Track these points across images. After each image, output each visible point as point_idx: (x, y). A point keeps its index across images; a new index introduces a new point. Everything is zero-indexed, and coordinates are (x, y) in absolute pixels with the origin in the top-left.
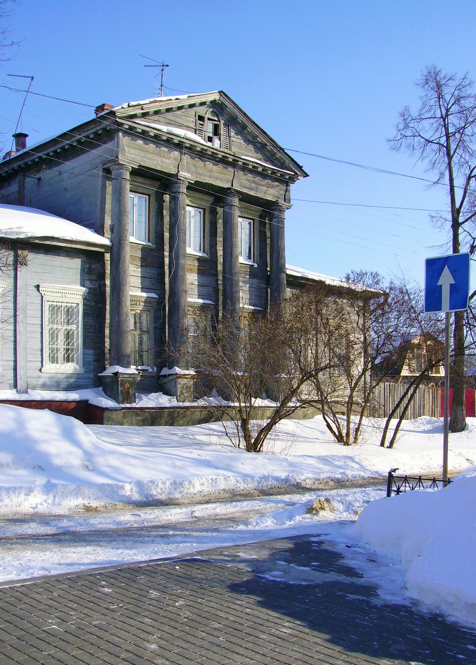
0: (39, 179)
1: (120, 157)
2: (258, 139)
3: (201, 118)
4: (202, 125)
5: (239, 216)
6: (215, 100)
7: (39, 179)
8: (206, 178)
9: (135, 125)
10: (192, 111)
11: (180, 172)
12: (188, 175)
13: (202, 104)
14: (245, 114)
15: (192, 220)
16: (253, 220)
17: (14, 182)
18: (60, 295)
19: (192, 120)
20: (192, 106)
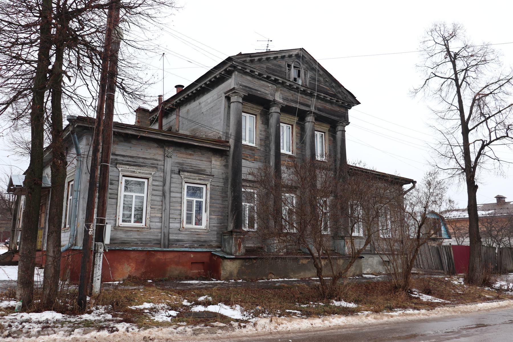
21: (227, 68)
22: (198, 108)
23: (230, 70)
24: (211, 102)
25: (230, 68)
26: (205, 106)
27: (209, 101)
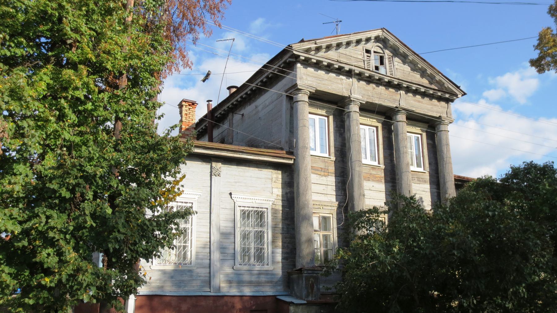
0: (243, 115)
1: (299, 82)
2: (419, 66)
3: (368, 51)
4: (369, 57)
5: (310, 113)
6: (379, 36)
7: (243, 115)
8: (376, 99)
9: (310, 56)
10: (360, 47)
11: (353, 95)
12: (360, 97)
13: (368, 40)
14: (405, 46)
15: (366, 134)
16: (421, 134)
17: (226, 121)
18: (251, 201)
19: (360, 53)
20: (358, 42)
21: (287, 59)
22: (254, 112)
23: (290, 62)
24: (269, 105)
25: (291, 60)
26: (263, 109)
27: (267, 103)
